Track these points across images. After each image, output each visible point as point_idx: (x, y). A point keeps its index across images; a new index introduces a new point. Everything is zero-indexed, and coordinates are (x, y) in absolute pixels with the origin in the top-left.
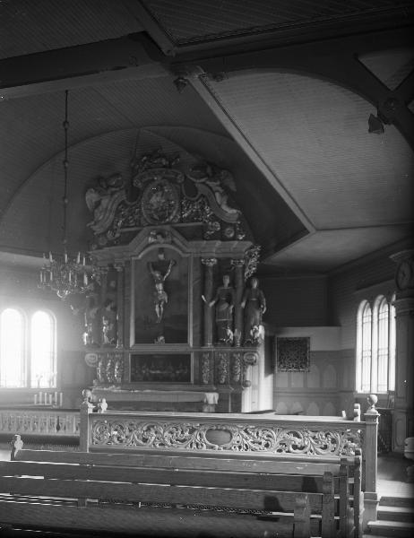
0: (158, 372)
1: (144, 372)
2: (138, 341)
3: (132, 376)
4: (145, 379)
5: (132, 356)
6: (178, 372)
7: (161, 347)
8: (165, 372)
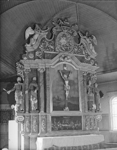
0: (66, 125)
1: (59, 125)
2: (55, 109)
3: (52, 128)
4: (59, 129)
5: (79, 110)
6: (76, 125)
7: (66, 113)
8: (69, 125)
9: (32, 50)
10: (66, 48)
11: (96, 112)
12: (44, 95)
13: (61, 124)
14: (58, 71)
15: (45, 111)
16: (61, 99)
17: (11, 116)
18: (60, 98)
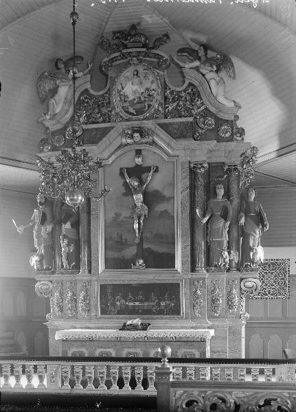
0: (137, 303)
1: (118, 303)
6: (163, 304)
8: (146, 304)
9: (59, 126)
10: (139, 106)
11: (239, 270)
12: (92, 235)
13: (123, 301)
14: (121, 169)
15: (90, 272)
16: (126, 240)
17: (285, 276)
18: (123, 238)
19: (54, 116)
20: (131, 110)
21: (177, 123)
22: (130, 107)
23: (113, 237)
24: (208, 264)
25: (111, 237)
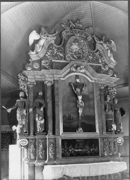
0: (80, 150)
6: (92, 150)
10: (78, 55)
16: (73, 117)
18: (71, 116)
19: (37, 53)
20: (75, 56)
21: (95, 66)
22: (74, 55)
23: (66, 116)
24: (107, 131)
25: (65, 116)
